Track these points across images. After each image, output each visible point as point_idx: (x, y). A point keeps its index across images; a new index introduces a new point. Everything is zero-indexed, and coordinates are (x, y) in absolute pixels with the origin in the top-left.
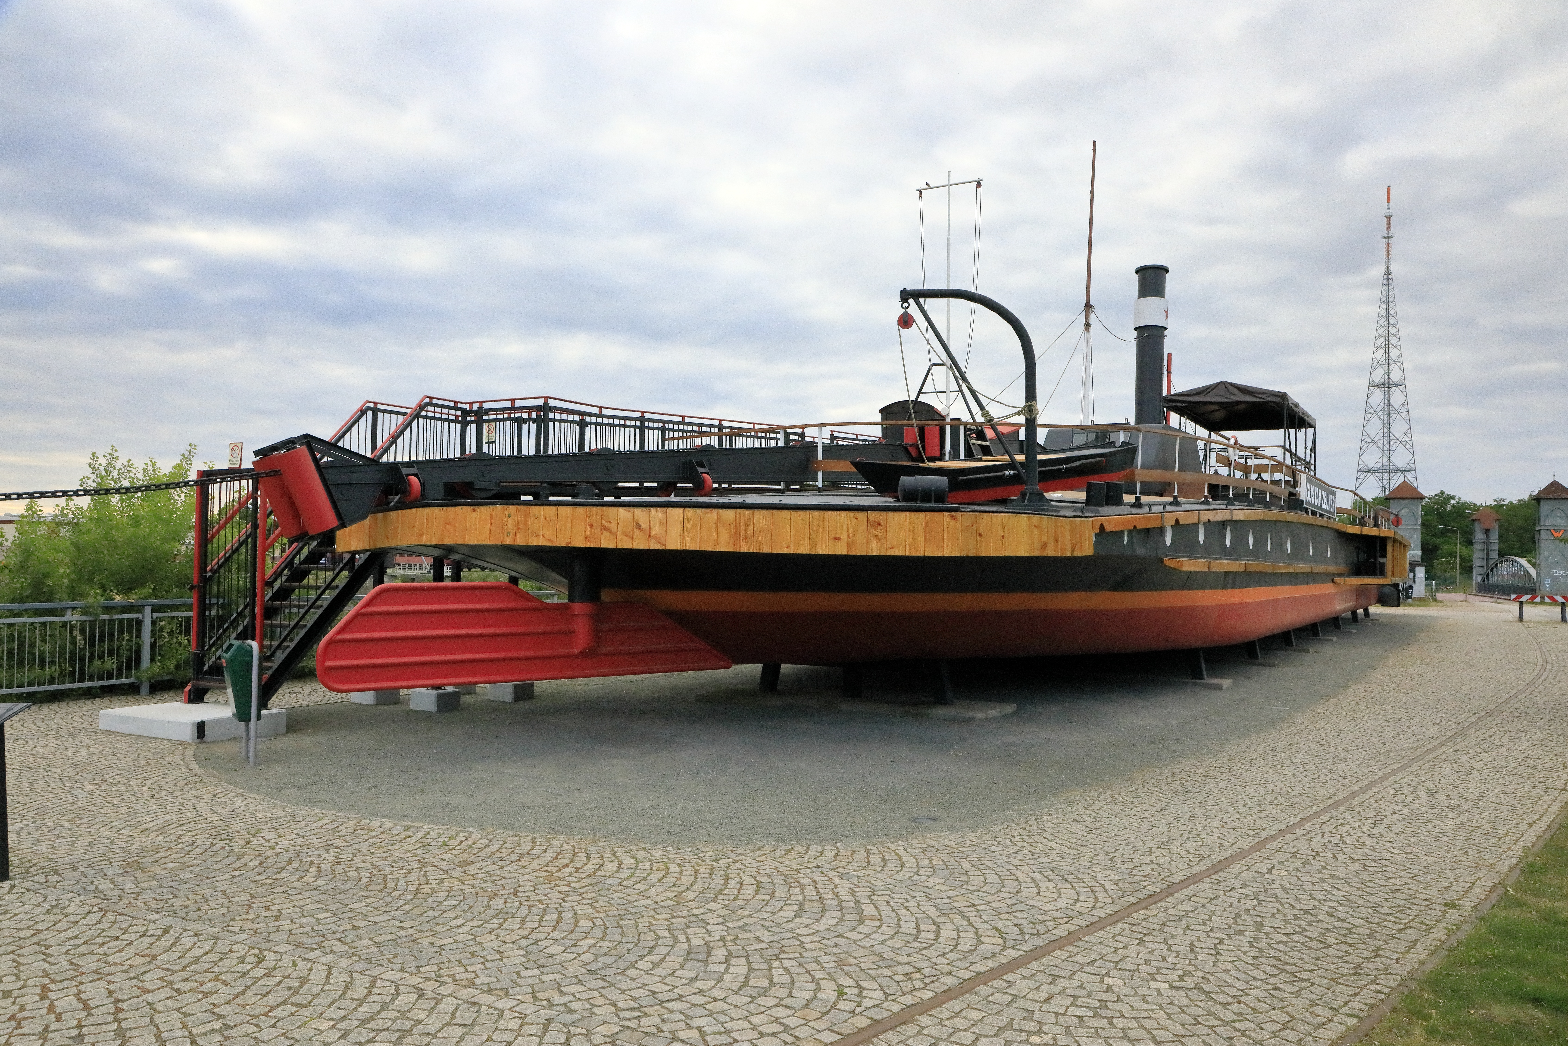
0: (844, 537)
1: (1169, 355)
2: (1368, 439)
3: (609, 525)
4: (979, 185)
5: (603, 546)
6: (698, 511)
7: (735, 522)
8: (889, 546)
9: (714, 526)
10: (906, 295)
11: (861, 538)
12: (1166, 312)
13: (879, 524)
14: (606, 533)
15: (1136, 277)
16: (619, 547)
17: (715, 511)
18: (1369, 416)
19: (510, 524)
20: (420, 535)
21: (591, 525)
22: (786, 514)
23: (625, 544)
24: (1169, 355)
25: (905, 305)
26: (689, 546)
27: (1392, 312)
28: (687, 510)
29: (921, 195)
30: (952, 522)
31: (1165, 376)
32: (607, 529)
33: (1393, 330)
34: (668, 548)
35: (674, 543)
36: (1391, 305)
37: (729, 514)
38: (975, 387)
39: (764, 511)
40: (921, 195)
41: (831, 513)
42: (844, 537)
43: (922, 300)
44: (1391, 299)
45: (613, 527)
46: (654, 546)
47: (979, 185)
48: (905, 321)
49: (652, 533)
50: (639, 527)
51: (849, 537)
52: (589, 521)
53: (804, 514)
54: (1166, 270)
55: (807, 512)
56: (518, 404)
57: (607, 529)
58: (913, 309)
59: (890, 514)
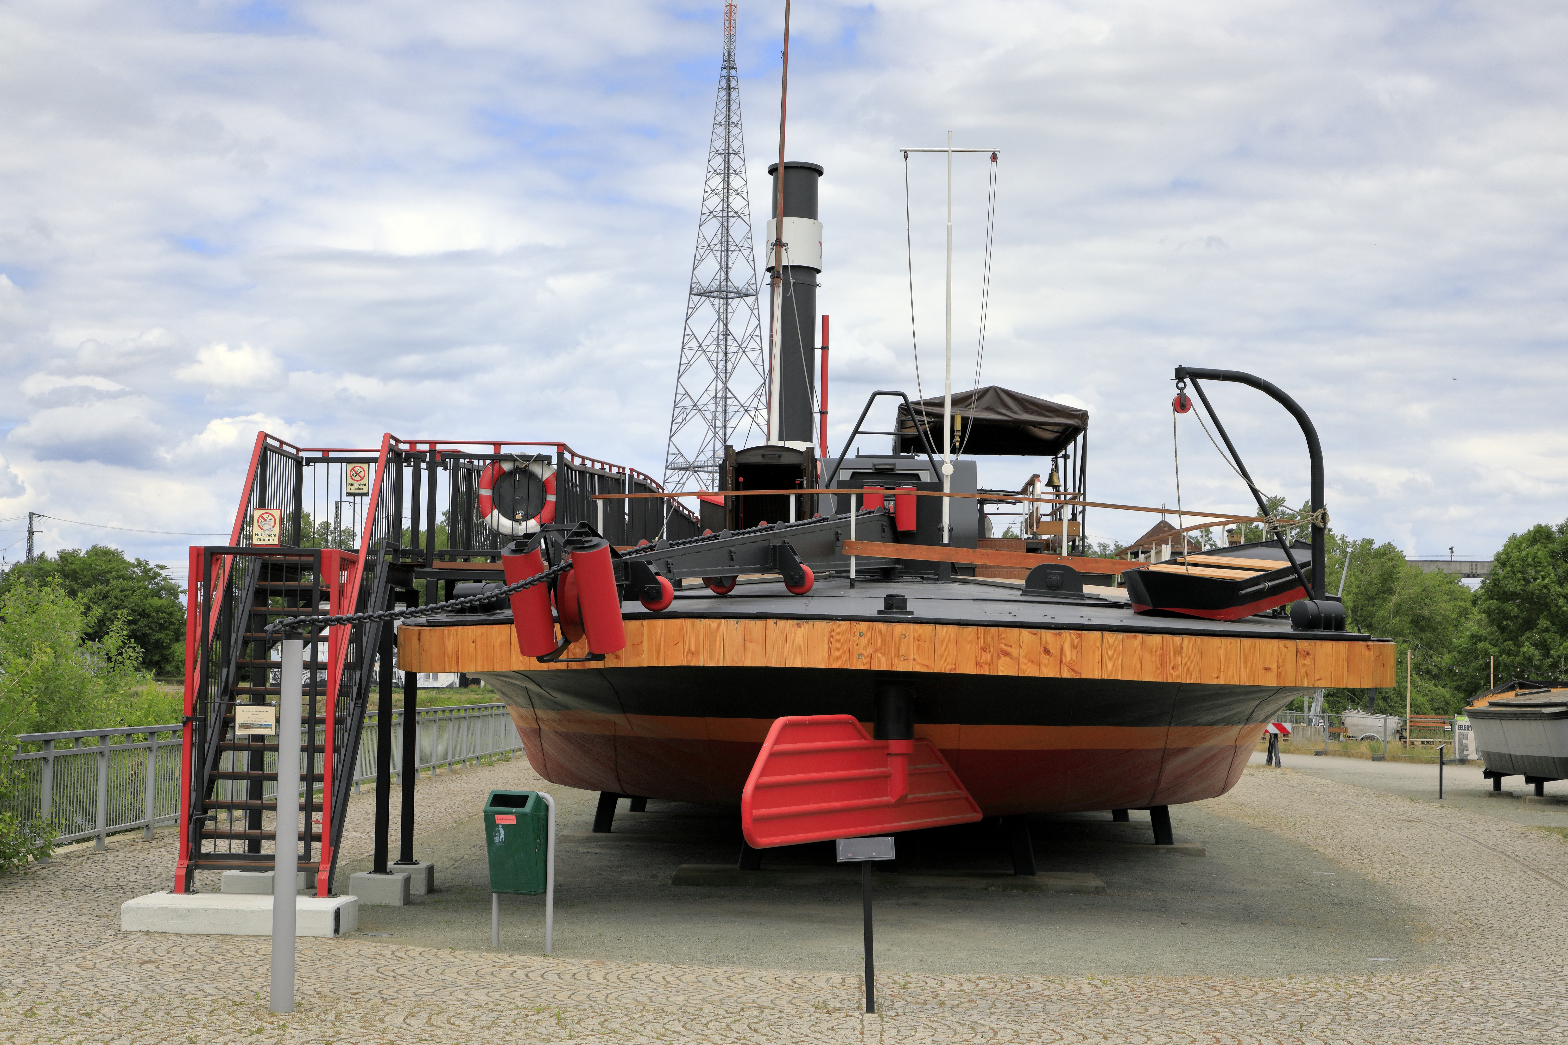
0: (1274, 667)
1: (825, 319)
2: (687, 402)
3: (1008, 649)
4: (994, 158)
5: (1001, 673)
6: (1120, 636)
7: (1162, 649)
8: (1317, 677)
9: (1138, 653)
10: (1181, 374)
11: (1290, 668)
12: (821, 243)
13: (1308, 654)
14: (1004, 659)
15: (771, 178)
16: (1022, 674)
17: (1140, 636)
18: (689, 353)
19: (862, 645)
20: (695, 653)
21: (984, 649)
22: (1216, 640)
23: (1030, 671)
24: (825, 319)
25: (1181, 385)
26: (1109, 675)
27: (735, 145)
28: (1106, 634)
29: (906, 157)
30: (1367, 652)
31: (818, 353)
32: (1006, 654)
33: (736, 182)
34: (1084, 676)
35: (1090, 672)
36: (735, 131)
37: (1156, 639)
38: (1258, 486)
39: (1194, 637)
40: (906, 157)
41: (1262, 641)
42: (1274, 667)
43: (1199, 381)
44: (734, 119)
45: (1014, 651)
46: (1066, 674)
47: (994, 158)
48: (1181, 405)
49: (1066, 659)
50: (1047, 651)
51: (1279, 668)
52: (981, 643)
53: (1236, 641)
54: (819, 171)
55: (1238, 640)
56: (504, 450)
57: (1006, 654)
58: (1190, 391)
59: (1318, 643)
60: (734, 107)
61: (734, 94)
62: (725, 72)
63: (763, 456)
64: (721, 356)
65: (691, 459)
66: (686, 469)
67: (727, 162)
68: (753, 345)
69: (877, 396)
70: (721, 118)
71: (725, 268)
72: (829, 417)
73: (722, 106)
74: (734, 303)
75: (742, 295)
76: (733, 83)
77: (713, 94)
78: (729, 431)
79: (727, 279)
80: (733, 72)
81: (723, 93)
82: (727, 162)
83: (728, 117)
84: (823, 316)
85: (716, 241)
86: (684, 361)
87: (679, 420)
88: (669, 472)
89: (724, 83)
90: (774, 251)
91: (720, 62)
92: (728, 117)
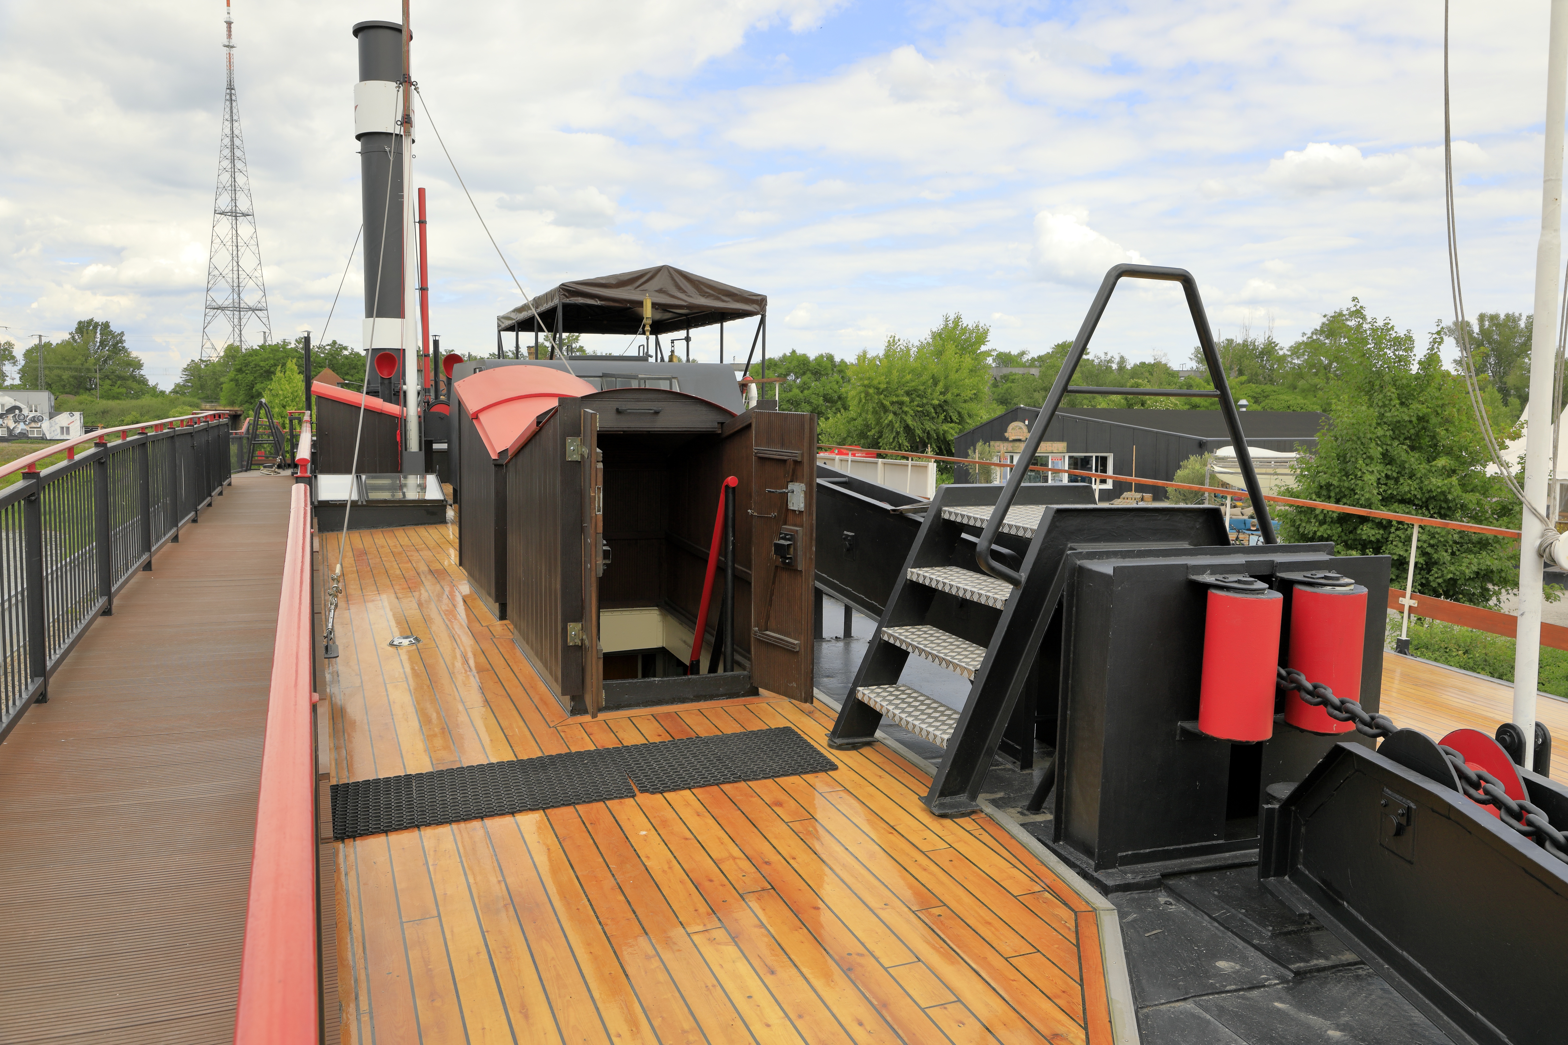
1: (422, 192)
2: (216, 273)
24: (422, 192)
60: (235, 111)
61: (234, 104)
62: (228, 91)
63: (618, 412)
64: (235, 248)
65: (220, 303)
66: (218, 309)
67: (232, 141)
68: (252, 242)
69: (1123, 280)
70: (228, 116)
71: (234, 200)
72: (430, 293)
73: (228, 109)
74: (240, 219)
75: (244, 215)
76: (234, 98)
77: (221, 105)
78: (241, 289)
79: (236, 206)
80: (233, 91)
81: (228, 103)
82: (232, 141)
83: (232, 116)
84: (420, 190)
85: (228, 184)
86: (213, 250)
87: (212, 282)
88: (208, 310)
89: (228, 97)
90: (401, 89)
91: (225, 85)
92: (232, 116)
